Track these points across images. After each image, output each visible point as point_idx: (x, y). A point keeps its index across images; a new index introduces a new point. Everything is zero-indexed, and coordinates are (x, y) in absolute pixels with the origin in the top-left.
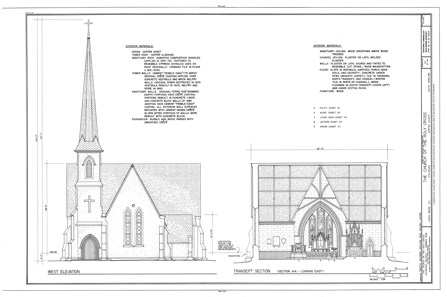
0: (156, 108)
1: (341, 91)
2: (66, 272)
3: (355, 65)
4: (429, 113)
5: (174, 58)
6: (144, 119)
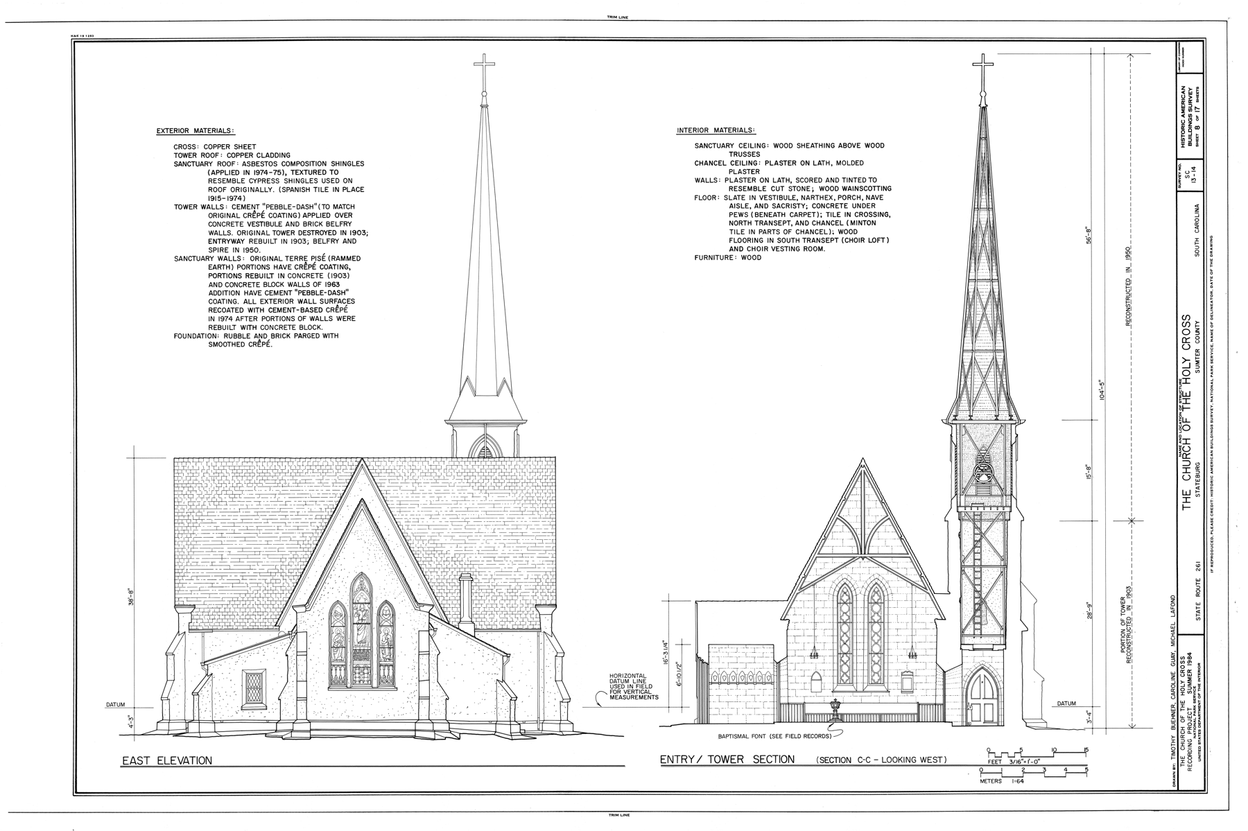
0: (240, 304)
1: (752, 257)
2: (171, 760)
3: (792, 185)
4: (1197, 316)
5: (292, 164)
6: (207, 336)
